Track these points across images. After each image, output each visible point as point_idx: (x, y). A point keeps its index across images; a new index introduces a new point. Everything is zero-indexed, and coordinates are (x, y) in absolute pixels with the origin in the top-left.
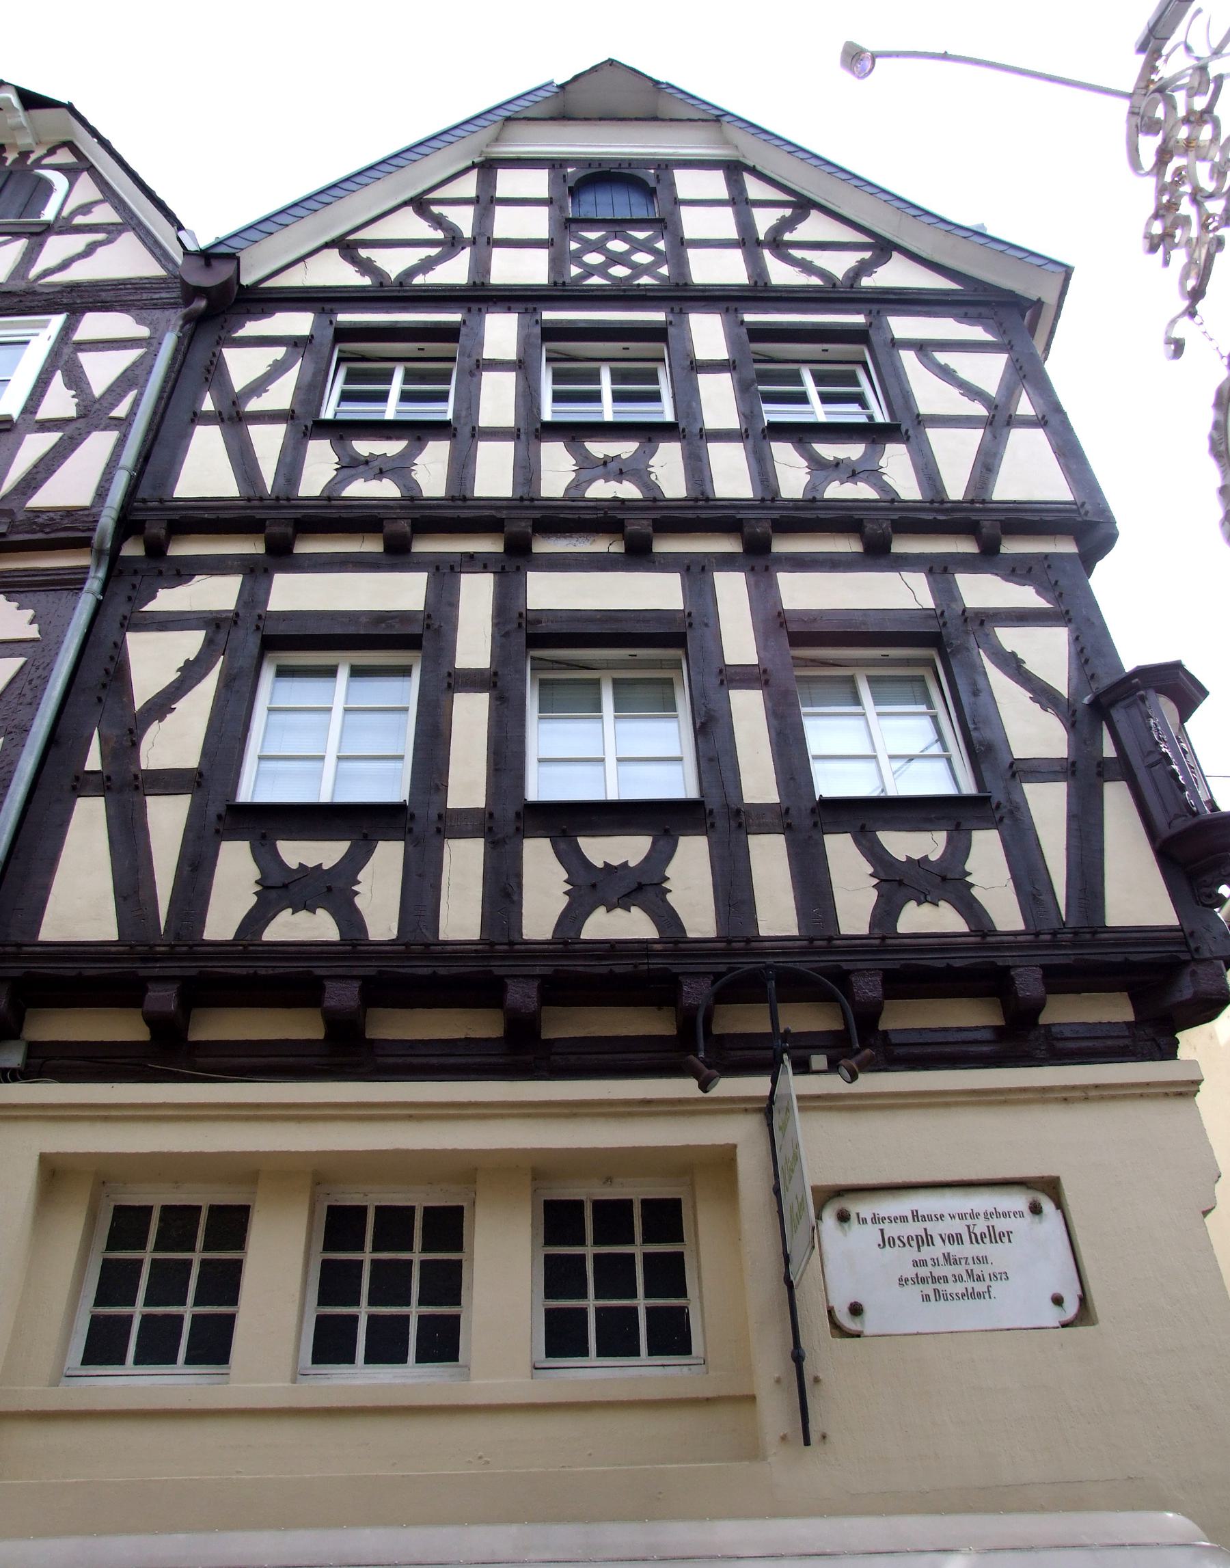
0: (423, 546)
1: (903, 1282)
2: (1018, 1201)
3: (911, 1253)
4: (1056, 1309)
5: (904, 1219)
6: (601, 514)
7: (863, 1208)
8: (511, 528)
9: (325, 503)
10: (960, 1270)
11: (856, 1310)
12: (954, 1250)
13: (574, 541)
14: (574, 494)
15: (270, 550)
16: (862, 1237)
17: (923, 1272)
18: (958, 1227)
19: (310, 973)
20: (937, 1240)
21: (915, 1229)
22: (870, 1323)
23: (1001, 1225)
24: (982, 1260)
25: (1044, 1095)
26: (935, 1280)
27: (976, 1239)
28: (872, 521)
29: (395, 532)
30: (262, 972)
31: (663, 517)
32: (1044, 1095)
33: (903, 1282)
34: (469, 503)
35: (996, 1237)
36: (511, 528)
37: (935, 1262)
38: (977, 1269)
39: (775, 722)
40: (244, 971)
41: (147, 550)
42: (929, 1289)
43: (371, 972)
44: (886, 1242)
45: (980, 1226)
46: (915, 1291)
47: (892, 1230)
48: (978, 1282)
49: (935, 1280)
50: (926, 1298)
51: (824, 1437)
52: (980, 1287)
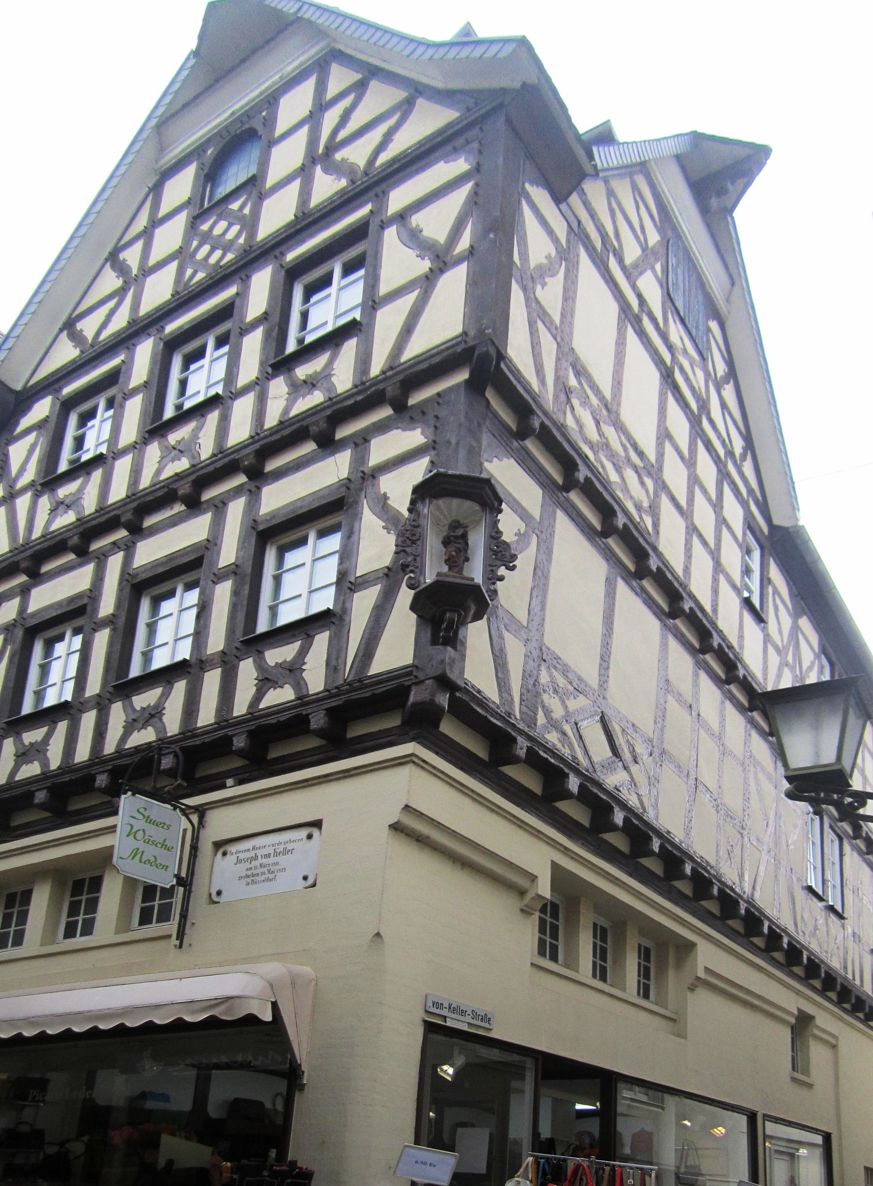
0: (342, 433)
1: (240, 878)
2: (303, 833)
3: (247, 865)
4: (304, 882)
5: (249, 850)
6: (166, 490)
7: (233, 848)
8: (314, 429)
9: (329, 403)
10: (265, 870)
11: (219, 893)
12: (265, 861)
13: (163, 511)
14: (156, 480)
15: (395, 410)
16: (231, 859)
17: (249, 873)
18: (270, 850)
19: (301, 714)
20: (260, 857)
21: (252, 854)
22: (223, 899)
23: (289, 846)
24: (277, 864)
25: (347, 774)
26: (253, 875)
27: (276, 854)
28: (313, 424)
29: (320, 432)
30: (207, 740)
31: (84, 530)
32: (347, 774)
33: (240, 878)
34: (138, 495)
35: (286, 852)
36: (314, 429)
37: (256, 868)
38: (272, 868)
39: (234, 599)
40: (368, 695)
41: (394, 410)
42: (249, 880)
43: (110, 767)
44: (239, 861)
45: (280, 848)
46: (244, 881)
47: (242, 856)
48: (271, 874)
49: (253, 875)
50: (248, 884)
51: (190, 945)
52: (271, 876)
